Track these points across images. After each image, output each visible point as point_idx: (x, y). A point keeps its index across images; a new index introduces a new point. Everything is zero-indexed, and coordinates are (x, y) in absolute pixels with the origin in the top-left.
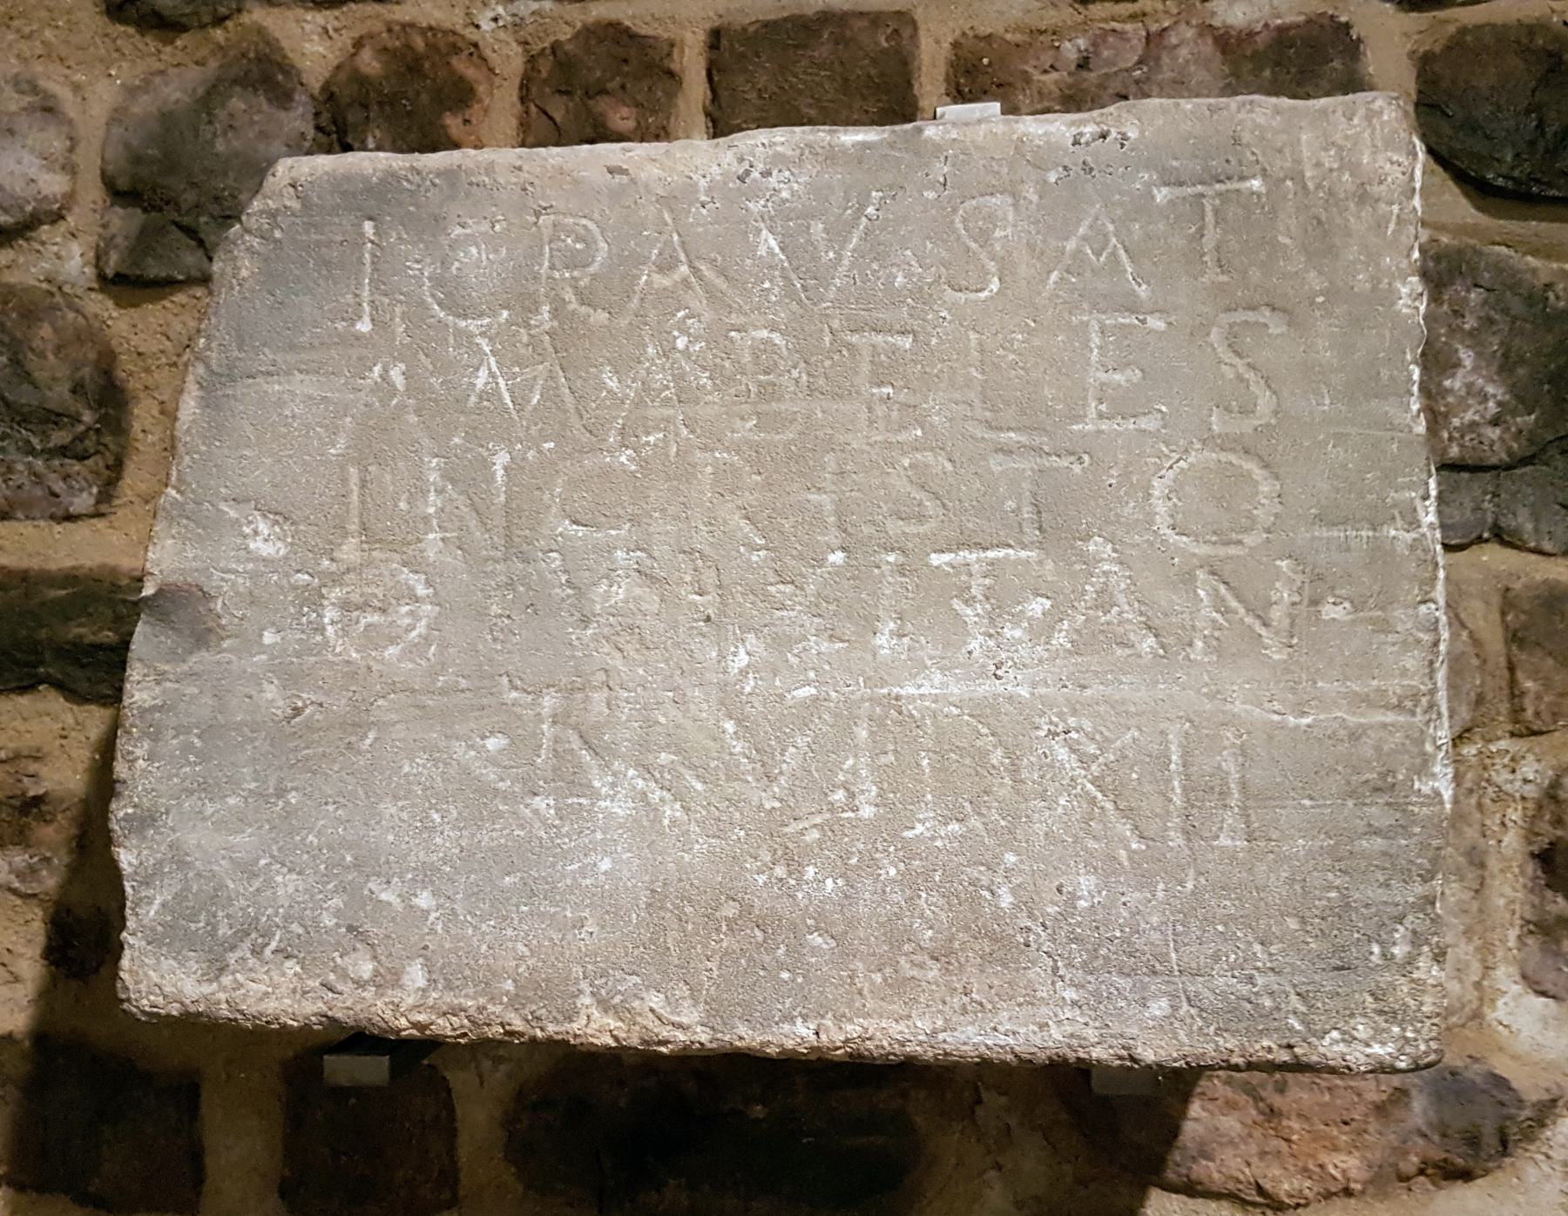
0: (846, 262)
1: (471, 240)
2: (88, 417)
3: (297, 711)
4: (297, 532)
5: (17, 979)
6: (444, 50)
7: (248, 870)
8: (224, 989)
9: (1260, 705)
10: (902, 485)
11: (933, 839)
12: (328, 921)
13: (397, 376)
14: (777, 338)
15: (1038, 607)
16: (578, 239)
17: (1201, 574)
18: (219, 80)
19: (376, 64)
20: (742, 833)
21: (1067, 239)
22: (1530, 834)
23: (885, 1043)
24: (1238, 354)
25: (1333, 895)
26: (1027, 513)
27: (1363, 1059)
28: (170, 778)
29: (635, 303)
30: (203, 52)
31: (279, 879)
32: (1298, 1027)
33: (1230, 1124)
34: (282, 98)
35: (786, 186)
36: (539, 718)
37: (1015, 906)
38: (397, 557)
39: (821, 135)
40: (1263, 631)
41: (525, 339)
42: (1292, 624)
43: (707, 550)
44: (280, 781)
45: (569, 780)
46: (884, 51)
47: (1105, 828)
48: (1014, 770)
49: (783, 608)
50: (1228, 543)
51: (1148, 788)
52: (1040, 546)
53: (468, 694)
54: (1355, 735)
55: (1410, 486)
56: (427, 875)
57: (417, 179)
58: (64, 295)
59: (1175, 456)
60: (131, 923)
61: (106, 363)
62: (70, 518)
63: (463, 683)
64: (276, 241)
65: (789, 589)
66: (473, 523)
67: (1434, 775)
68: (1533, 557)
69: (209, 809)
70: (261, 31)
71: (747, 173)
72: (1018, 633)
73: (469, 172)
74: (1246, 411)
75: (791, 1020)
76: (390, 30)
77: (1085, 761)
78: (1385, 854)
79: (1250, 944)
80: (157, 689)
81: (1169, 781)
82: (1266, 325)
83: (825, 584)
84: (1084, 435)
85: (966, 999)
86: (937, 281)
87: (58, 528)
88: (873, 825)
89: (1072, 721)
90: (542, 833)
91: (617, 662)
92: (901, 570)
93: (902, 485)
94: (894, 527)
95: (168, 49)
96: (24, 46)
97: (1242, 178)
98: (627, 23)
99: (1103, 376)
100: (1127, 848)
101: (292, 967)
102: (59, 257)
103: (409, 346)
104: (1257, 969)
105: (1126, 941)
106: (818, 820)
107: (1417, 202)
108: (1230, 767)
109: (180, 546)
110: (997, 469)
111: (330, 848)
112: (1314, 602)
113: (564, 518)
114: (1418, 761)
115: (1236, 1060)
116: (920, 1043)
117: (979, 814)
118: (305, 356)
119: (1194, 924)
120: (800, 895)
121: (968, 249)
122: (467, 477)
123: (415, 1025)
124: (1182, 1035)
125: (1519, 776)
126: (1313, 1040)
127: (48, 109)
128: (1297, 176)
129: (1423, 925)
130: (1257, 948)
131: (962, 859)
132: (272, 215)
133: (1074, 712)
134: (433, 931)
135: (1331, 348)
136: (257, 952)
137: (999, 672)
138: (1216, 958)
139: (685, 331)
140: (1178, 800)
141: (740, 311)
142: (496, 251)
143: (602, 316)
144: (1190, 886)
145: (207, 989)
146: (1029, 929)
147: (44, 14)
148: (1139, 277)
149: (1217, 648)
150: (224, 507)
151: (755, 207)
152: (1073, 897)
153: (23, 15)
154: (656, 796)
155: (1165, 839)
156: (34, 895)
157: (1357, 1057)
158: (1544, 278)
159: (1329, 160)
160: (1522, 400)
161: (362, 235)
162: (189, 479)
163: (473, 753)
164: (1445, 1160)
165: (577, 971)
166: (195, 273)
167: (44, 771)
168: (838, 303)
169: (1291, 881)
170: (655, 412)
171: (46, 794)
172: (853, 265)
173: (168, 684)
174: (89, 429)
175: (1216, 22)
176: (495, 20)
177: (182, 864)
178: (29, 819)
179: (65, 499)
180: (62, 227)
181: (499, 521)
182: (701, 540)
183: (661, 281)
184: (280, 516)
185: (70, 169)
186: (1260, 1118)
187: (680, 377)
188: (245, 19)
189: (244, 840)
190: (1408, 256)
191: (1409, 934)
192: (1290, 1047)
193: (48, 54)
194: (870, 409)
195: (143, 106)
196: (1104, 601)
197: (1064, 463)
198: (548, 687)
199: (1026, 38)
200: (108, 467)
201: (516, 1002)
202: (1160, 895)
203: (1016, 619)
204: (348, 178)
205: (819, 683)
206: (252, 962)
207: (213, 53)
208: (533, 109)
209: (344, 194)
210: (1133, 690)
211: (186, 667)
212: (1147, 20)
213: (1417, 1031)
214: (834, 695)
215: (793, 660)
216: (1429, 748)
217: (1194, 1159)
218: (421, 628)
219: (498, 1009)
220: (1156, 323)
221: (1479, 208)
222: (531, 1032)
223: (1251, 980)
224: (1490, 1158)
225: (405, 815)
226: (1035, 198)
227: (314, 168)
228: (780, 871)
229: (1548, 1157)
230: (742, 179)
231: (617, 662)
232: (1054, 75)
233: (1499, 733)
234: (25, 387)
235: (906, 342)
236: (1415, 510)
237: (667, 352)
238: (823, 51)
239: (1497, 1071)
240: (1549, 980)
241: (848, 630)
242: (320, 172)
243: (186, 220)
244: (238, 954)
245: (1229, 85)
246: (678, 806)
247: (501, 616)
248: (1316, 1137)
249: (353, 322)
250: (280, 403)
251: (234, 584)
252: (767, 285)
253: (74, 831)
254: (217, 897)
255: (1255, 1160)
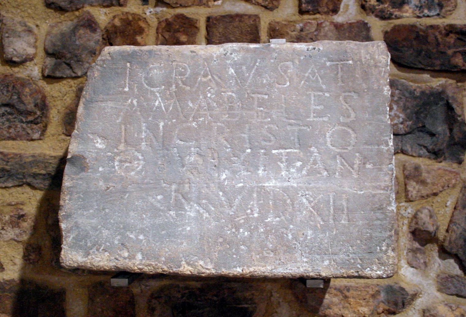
0: (251, 76)
1: (155, 68)
2: (38, 113)
3: (108, 188)
4: (108, 142)
5: (15, 264)
6: (137, 19)
7: (95, 229)
8: (89, 259)
9: (351, 189)
10: (264, 132)
11: (272, 222)
12: (116, 242)
13: (135, 102)
14: (234, 95)
15: (299, 164)
16: (182, 69)
17: (338, 157)
18: (77, 25)
19: (119, 23)
20: (224, 221)
21: (305, 73)
22: (410, 227)
23: (259, 273)
24: (347, 103)
25: (368, 235)
26: (296, 140)
27: (375, 275)
28: (75, 205)
29: (197, 85)
30: (73, 17)
31: (103, 231)
32: (360, 267)
33: (335, 300)
34: (94, 30)
35: (236, 57)
36: (171, 191)
37: (292, 238)
38: (134, 149)
39: (245, 45)
40: (352, 171)
41: (168, 93)
42: (359, 169)
43: (215, 148)
44: (104, 206)
45: (179, 207)
46: (252, 25)
47: (315, 219)
48: (293, 204)
49: (235, 163)
50: (344, 149)
51: (325, 209)
52: (299, 149)
53: (153, 185)
54: (374, 196)
55: (387, 136)
56: (142, 231)
57: (141, 53)
58: (33, 80)
59: (332, 127)
60: (64, 243)
61: (44, 98)
62: (32, 140)
63: (151, 182)
64: (104, 67)
65: (236, 158)
66: (154, 140)
67: (392, 206)
68: (410, 157)
69: (85, 213)
70: (89, 13)
71: (226, 54)
72: (294, 170)
73: (155, 51)
74: (349, 117)
75: (236, 267)
76: (123, 14)
77: (310, 202)
78: (381, 225)
79: (348, 246)
80: (72, 182)
81: (330, 207)
82: (353, 96)
83: (246, 157)
84: (310, 121)
85: (280, 261)
86: (274, 82)
87: (29, 143)
88: (257, 219)
89: (307, 192)
90: (172, 220)
91: (191, 176)
92: (265, 154)
93: (264, 132)
94: (264, 143)
95: (63, 16)
96: (22, 14)
97: (348, 61)
98: (185, 14)
99: (315, 107)
100: (320, 224)
101: (107, 254)
102: (31, 70)
103: (138, 95)
104: (350, 253)
105: (319, 247)
106: (243, 217)
107: (388, 68)
108: (344, 203)
109: (78, 145)
110: (289, 129)
111: (117, 224)
112: (364, 164)
113: (178, 139)
114: (388, 202)
115: (345, 275)
116: (268, 273)
117: (284, 216)
118: (111, 97)
119: (335, 242)
120: (239, 236)
121: (281, 75)
122: (153, 128)
123: (139, 269)
124: (332, 269)
125: (407, 212)
126: (363, 270)
127: (30, 31)
128: (360, 60)
129: (390, 242)
130: (350, 248)
131: (279, 227)
132: (104, 61)
133: (308, 190)
134: (144, 245)
135: (368, 102)
136: (98, 250)
137: (289, 180)
138: (340, 250)
139: (210, 92)
140: (332, 211)
141: (224, 88)
142: (161, 71)
143: (188, 88)
144: (334, 233)
145: (84, 259)
146: (296, 244)
147: (28, 5)
148: (323, 83)
149: (342, 175)
150: (89, 135)
151: (228, 62)
152: (307, 236)
153: (23, 5)
154: (202, 211)
155: (329, 221)
156: (21, 242)
157: (374, 274)
158: (414, 88)
159: (368, 57)
160: (409, 118)
161: (126, 66)
162: (80, 128)
163: (154, 200)
164: (389, 309)
165: (181, 255)
166: (69, 76)
167: (24, 208)
168: (250, 86)
169: (358, 231)
170: (202, 112)
171: (25, 214)
172: (253, 77)
173: (74, 181)
174: (39, 116)
175: (335, 21)
176: (150, 12)
177: (78, 227)
178: (20, 221)
179: (31, 135)
180: (33, 62)
181: (161, 140)
182: (214, 145)
183: (204, 80)
184: (104, 138)
185: (35, 47)
186: (343, 298)
187: (209, 104)
188: (85, 9)
189: (94, 221)
190: (387, 81)
191: (386, 245)
192: (358, 272)
193: (29, 16)
194: (257, 113)
195: (55, 31)
196: (315, 162)
197: (305, 128)
198: (174, 183)
199: (287, 23)
200: (43, 127)
201: (165, 263)
202: (327, 235)
203: (293, 167)
204: (124, 52)
205: (244, 182)
206: (96, 252)
207: (75, 18)
208: (160, 35)
209: (122, 56)
210: (321, 185)
211: (79, 177)
212: (318, 20)
213: (388, 268)
214: (248, 185)
215: (237, 177)
216: (391, 199)
217: (326, 309)
218: (140, 167)
219: (160, 265)
220: (327, 95)
221: (398, 70)
222: (169, 271)
223: (348, 256)
224: (400, 309)
225: (136, 215)
226: (298, 63)
227: (114, 49)
228: (234, 230)
229: (414, 309)
230: (225, 55)
231: (191, 176)
232: (294, 33)
233: (402, 201)
234: (22, 105)
235: (266, 97)
236: (388, 142)
237: (205, 97)
238: (236, 24)
239: (402, 286)
240: (414, 263)
241: (252, 169)
242: (116, 50)
243: (68, 62)
244: (93, 250)
245: (338, 37)
246: (207, 214)
247: (161, 164)
248: (357, 303)
249: (124, 88)
250: (104, 109)
251: (91, 156)
252: (231, 81)
253: (33, 224)
254: (87, 236)
255: (342, 309)
